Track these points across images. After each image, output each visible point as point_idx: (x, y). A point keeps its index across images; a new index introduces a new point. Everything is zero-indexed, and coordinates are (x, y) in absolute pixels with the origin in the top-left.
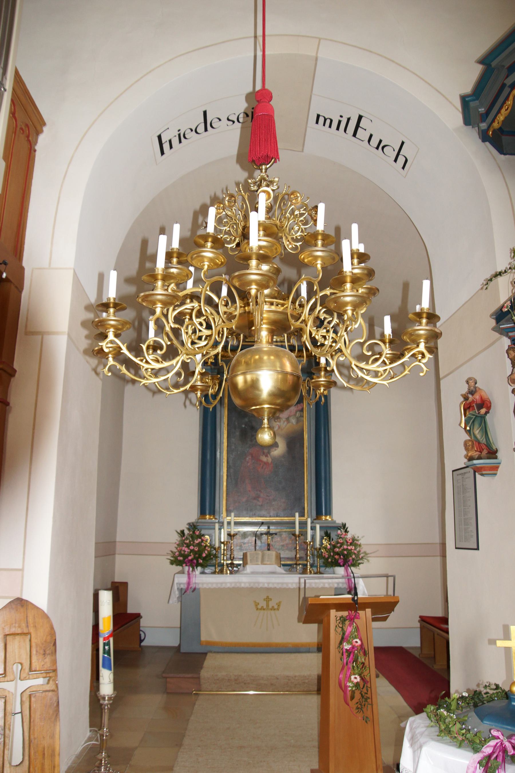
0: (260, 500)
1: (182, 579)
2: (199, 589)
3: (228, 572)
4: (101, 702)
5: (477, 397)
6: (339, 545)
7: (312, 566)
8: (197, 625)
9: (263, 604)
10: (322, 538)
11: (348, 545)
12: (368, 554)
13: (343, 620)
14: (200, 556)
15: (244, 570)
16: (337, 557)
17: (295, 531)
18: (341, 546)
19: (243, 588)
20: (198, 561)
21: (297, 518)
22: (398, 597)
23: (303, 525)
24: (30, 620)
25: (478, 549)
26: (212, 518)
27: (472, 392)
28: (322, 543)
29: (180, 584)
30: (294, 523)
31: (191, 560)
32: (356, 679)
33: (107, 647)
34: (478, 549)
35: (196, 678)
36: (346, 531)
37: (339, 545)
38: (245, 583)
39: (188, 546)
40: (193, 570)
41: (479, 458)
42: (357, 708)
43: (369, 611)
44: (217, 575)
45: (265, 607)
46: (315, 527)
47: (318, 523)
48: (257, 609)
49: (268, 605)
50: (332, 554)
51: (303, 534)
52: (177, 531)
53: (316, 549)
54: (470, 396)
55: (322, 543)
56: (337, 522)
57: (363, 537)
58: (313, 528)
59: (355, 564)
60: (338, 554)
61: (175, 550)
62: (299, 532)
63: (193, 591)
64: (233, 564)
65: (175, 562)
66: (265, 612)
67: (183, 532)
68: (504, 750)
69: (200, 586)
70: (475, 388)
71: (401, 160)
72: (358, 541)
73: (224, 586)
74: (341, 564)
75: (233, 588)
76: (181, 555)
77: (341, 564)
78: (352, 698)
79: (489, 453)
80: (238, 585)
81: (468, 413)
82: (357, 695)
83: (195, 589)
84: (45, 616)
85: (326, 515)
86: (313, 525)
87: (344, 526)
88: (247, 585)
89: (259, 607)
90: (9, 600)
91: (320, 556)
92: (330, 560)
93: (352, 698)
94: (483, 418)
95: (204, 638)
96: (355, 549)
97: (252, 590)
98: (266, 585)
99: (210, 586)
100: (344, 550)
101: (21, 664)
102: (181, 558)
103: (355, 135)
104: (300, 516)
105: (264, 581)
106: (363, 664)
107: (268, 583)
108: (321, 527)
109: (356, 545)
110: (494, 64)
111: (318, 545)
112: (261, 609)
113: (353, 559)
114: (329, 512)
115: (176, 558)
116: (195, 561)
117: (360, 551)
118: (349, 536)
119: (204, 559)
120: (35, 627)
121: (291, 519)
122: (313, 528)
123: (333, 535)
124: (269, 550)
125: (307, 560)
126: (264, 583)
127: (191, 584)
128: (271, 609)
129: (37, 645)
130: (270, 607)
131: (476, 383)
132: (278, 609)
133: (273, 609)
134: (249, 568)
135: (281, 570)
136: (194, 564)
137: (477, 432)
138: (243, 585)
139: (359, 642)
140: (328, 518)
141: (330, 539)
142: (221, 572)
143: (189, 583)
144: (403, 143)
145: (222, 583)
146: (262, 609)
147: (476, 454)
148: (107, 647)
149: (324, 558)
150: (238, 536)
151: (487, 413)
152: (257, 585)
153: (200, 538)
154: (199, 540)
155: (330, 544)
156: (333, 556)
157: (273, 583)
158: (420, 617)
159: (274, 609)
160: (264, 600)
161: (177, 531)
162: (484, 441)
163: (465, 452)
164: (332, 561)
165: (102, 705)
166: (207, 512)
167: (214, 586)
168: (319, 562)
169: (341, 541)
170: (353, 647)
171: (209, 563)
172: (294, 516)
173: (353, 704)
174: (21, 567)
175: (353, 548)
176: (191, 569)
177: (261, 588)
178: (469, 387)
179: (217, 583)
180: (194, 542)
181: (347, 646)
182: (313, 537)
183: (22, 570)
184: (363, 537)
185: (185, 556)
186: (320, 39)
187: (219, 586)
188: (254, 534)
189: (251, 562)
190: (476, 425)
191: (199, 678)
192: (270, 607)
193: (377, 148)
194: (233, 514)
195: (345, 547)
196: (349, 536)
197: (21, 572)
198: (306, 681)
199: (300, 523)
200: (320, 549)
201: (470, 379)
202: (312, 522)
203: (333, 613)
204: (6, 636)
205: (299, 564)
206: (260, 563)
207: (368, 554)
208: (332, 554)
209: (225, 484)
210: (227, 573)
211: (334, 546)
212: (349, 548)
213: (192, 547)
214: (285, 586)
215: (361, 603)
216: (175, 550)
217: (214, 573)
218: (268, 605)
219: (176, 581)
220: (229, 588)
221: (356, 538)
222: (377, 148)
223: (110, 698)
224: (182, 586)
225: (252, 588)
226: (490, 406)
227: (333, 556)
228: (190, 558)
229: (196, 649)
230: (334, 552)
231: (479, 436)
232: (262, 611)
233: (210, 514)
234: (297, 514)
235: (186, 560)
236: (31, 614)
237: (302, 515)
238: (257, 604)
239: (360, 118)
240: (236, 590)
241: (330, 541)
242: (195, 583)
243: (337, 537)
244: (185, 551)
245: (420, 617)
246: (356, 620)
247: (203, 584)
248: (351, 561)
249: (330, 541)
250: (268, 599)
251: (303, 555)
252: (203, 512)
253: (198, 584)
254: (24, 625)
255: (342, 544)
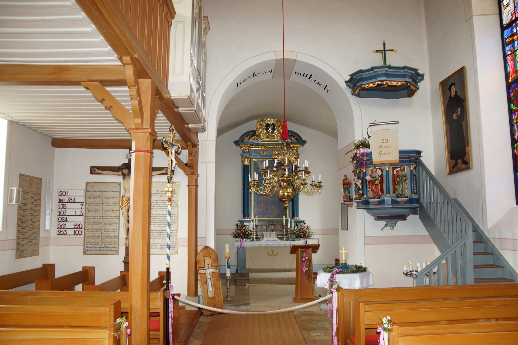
0: (268, 210)
1: (238, 244)
2: (245, 247)
3: (256, 240)
4: (227, 279)
5: (347, 181)
6: (302, 229)
7: (290, 238)
8: (245, 262)
9: (271, 253)
10: (294, 226)
11: (305, 229)
12: (314, 233)
13: (303, 252)
14: (245, 234)
15: (262, 240)
16: (301, 234)
17: (283, 224)
18: (302, 230)
19: (263, 247)
20: (244, 236)
21: (284, 218)
22: (320, 245)
23: (287, 221)
24: (210, 252)
25: (347, 230)
26: (248, 218)
27: (346, 180)
28: (294, 229)
29: (237, 245)
30: (283, 220)
31: (242, 236)
32: (307, 269)
33: (228, 262)
34: (347, 230)
35: (247, 280)
36: (305, 224)
37: (302, 229)
38: (264, 245)
39: (240, 230)
40: (243, 240)
41: (347, 201)
42: (307, 278)
43: (311, 249)
44: (252, 242)
45: (272, 254)
46: (292, 222)
47: (293, 220)
48: (269, 255)
49: (273, 253)
50: (299, 233)
51: (287, 225)
52: (235, 224)
53: (292, 231)
54: (345, 181)
55: (294, 229)
56: (301, 220)
57: (312, 226)
58: (291, 223)
59: (308, 237)
60: (301, 232)
61: (234, 232)
62: (285, 224)
63: (243, 248)
64: (258, 237)
65: (235, 236)
66: (272, 256)
67: (237, 224)
68: (337, 272)
69: (246, 246)
70: (347, 178)
71: (326, 90)
72: (309, 227)
73: (255, 246)
74: (303, 237)
75: (259, 247)
76: (237, 234)
77: (303, 237)
78: (306, 275)
79: (350, 199)
80: (261, 245)
81: (344, 186)
82: (307, 274)
83: (243, 247)
84: (214, 251)
85: (296, 217)
86: (291, 221)
87: (304, 221)
88: (265, 245)
89: (269, 254)
90: (204, 247)
91: (294, 234)
92: (298, 235)
93: (306, 275)
94: (349, 188)
95: (247, 267)
96: (308, 231)
97: (267, 247)
98: (272, 245)
99: (249, 246)
100: (304, 231)
101: (209, 265)
102: (238, 235)
103: (309, 78)
104: (285, 217)
105: (271, 244)
106: (309, 264)
107: (273, 245)
108: (294, 222)
109: (308, 229)
110: (354, 77)
111: (293, 229)
112: (270, 255)
113: (307, 235)
114: (297, 216)
115: (235, 235)
116: (243, 236)
117: (310, 231)
118: (306, 225)
119: (247, 235)
120: (212, 254)
121: (281, 218)
122: (291, 223)
123: (299, 225)
124: (272, 231)
125: (288, 236)
126: (271, 245)
127: (242, 245)
128: (274, 255)
129: (213, 259)
130: (274, 254)
131: (347, 177)
132: (277, 255)
133: (275, 255)
134: (264, 239)
135: (278, 239)
136: (243, 237)
137: (346, 192)
138: (263, 246)
139: (308, 258)
140: (297, 218)
141: (298, 227)
142: (253, 240)
143: (241, 245)
144: (327, 86)
145: (254, 245)
146: (271, 255)
147: (345, 200)
148: (228, 262)
149: (295, 234)
150: (259, 226)
151: (350, 187)
152: (268, 245)
153: (245, 227)
154: (245, 228)
155: (298, 229)
156: (299, 234)
157: (275, 245)
158: (336, 259)
159: (276, 255)
160: (271, 251)
161: (235, 224)
162: (349, 196)
163: (343, 199)
164: (298, 236)
165: (227, 279)
166: (246, 216)
167: (251, 246)
168: (293, 236)
169: (302, 227)
170: (306, 260)
171: (248, 237)
172: (283, 217)
173: (306, 277)
174: (205, 237)
175: (307, 230)
176: (242, 239)
177: (270, 246)
178: (345, 178)
179: (252, 245)
180: (242, 229)
181: (304, 259)
182: (291, 226)
183: (206, 238)
184: (312, 226)
185: (239, 235)
186: (297, 52)
187: (253, 246)
188: (266, 225)
189: (265, 236)
190: (346, 190)
191: (249, 280)
192: (274, 254)
193: (318, 84)
194: (257, 217)
195: (304, 230)
196: (306, 225)
197: (205, 238)
198: (289, 280)
199: (285, 220)
200: (294, 231)
201: (345, 175)
202: (290, 220)
203: (300, 249)
204: (204, 257)
205: (285, 237)
206: (269, 237)
207: (314, 233)
208: (299, 233)
209: (253, 204)
210: (255, 241)
211: (300, 230)
212: (306, 230)
213: (242, 231)
214: (280, 246)
215: (308, 246)
216: (234, 232)
217: (251, 241)
218: (273, 253)
219: (236, 244)
220: (257, 247)
221: (309, 226)
222: (318, 84)
223: (229, 278)
224: (238, 246)
225: (266, 246)
226: (351, 184)
227: (299, 234)
228: (241, 235)
229: (244, 271)
230: (299, 232)
231: (347, 194)
232: (271, 256)
233: (247, 217)
234: (284, 216)
235: (240, 236)
236: (210, 250)
237: (286, 217)
238: (268, 253)
239: (311, 75)
240: (260, 247)
241: (298, 227)
242: (244, 245)
243: (301, 226)
244: (239, 232)
245: (336, 259)
246: (307, 252)
247: (247, 245)
248: (306, 235)
249: (298, 227)
250: (273, 251)
251: (287, 234)
252: (244, 216)
253: (245, 245)
254: (209, 254)
255: (303, 229)
